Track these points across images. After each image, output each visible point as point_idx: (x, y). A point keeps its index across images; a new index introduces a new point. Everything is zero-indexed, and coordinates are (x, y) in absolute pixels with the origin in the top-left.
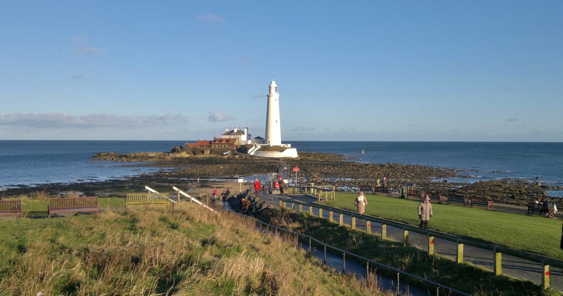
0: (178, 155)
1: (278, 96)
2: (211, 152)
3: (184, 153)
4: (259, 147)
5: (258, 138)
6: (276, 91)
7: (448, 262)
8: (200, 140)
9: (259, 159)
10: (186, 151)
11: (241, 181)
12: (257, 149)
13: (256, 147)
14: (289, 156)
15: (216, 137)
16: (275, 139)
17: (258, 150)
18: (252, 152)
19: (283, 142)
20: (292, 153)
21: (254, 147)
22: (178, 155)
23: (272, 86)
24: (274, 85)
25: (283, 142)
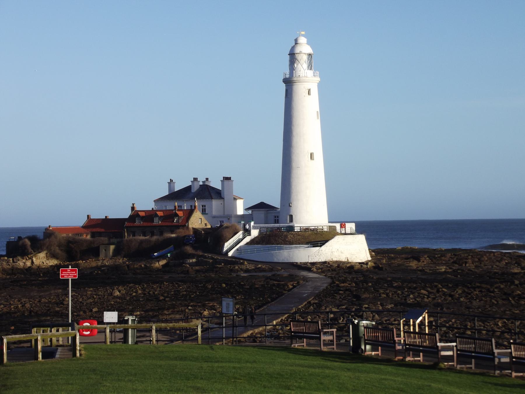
0: (22, 263)
1: (318, 79)
2: (117, 252)
3: (42, 255)
4: (255, 233)
5: (262, 206)
6: (310, 67)
7: (317, 350)
8: (110, 217)
9: (251, 267)
10: (49, 249)
11: (218, 344)
12: (248, 239)
13: (247, 232)
14: (343, 259)
15: (138, 208)
16: (311, 210)
17: (253, 242)
18: (232, 245)
19: (329, 222)
20: (351, 249)
21: (240, 235)
22: (22, 263)
23: (298, 50)
24: (304, 48)
25: (329, 222)
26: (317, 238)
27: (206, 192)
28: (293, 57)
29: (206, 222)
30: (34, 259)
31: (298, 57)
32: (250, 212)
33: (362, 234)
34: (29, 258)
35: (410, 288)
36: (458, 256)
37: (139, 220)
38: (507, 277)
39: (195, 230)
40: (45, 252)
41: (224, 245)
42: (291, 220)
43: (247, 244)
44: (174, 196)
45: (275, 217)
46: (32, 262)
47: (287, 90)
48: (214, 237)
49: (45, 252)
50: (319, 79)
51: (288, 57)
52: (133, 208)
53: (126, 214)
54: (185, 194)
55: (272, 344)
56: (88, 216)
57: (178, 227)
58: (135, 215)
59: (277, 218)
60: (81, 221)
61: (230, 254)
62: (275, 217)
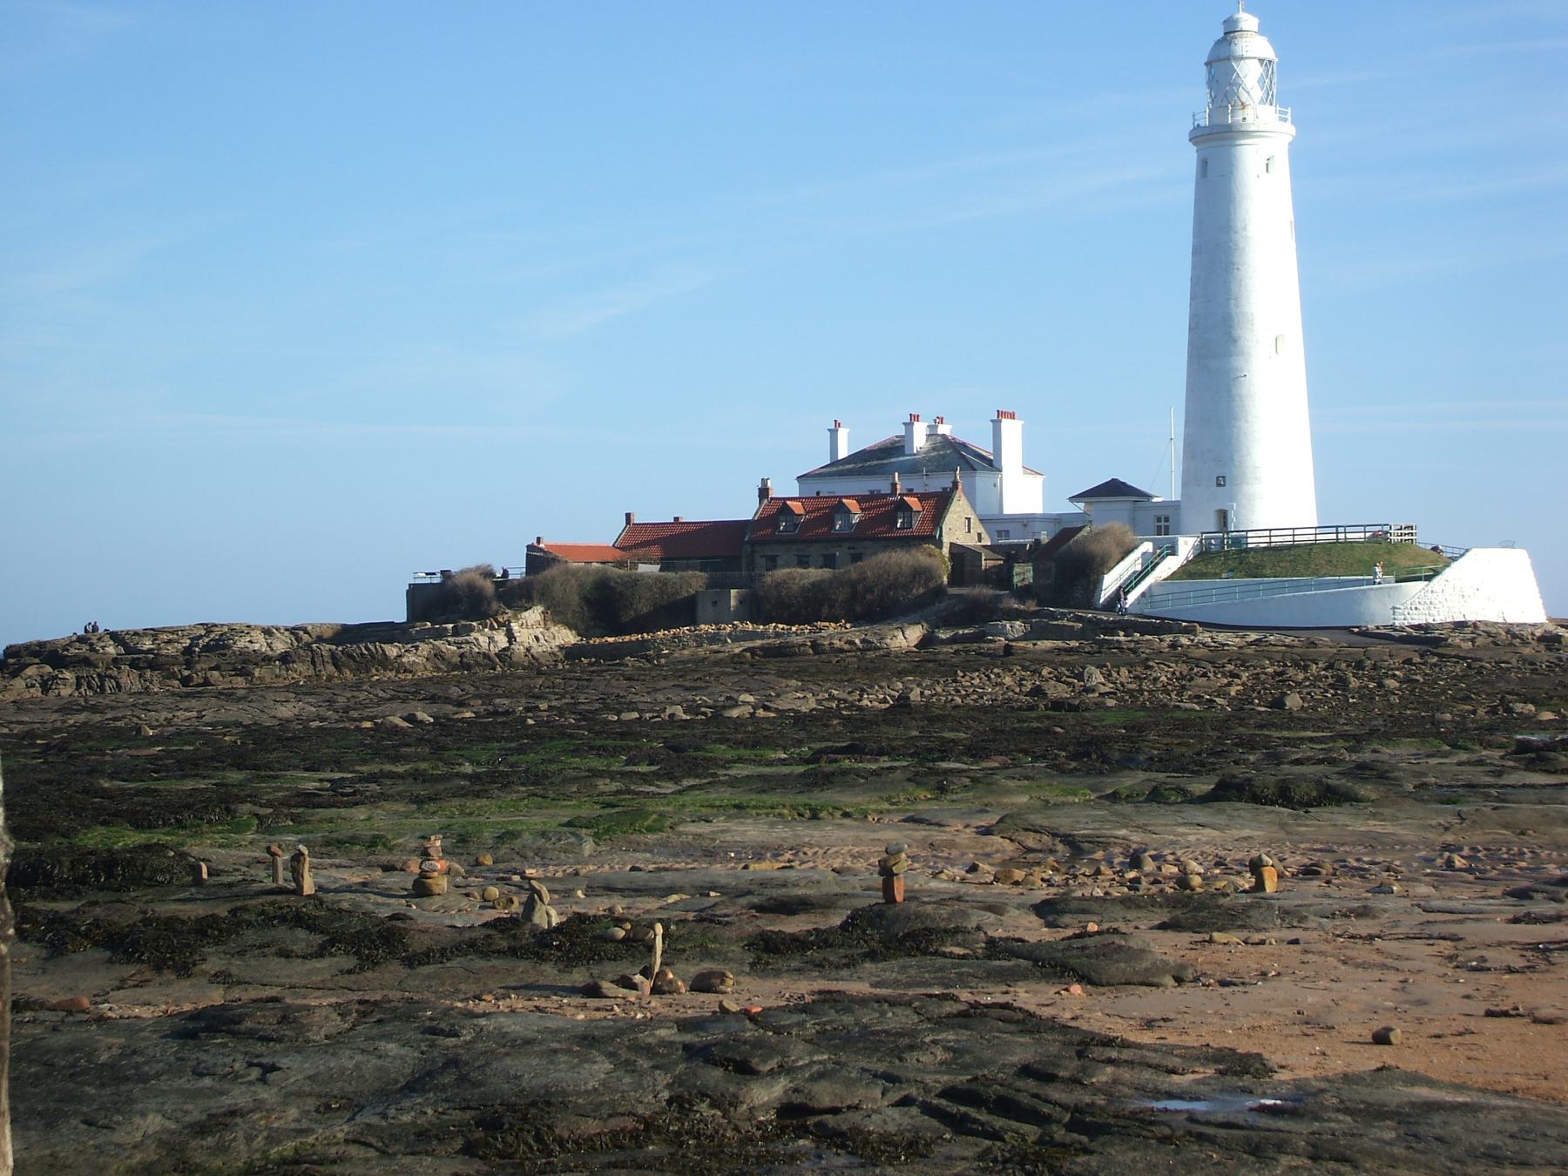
12: (1170, 565)
28: (1220, 63)
29: (981, 529)
30: (515, 626)
32: (1080, 507)
33: (1509, 544)
34: (501, 625)
37: (775, 530)
39: (960, 555)
40: (540, 609)
41: (1098, 583)
43: (1173, 576)
45: (1159, 520)
46: (511, 636)
47: (1204, 166)
49: (540, 609)
50: (1292, 130)
52: (764, 492)
53: (745, 509)
55: (340, 896)
56: (628, 516)
58: (775, 511)
59: (1163, 524)
60: (605, 533)
62: (1159, 520)
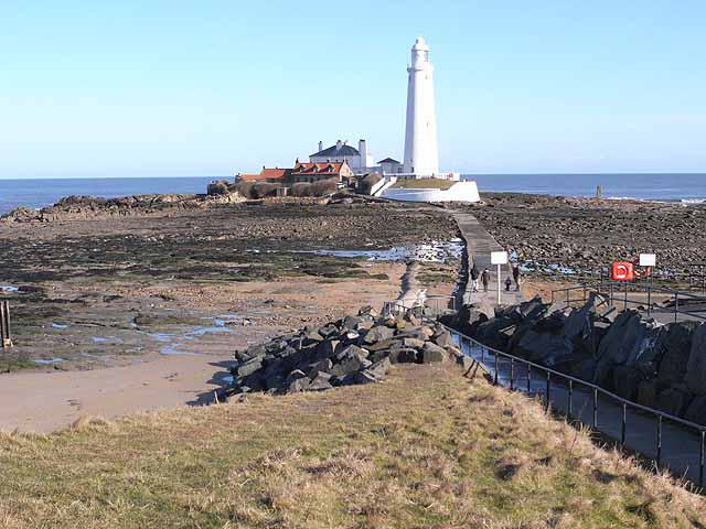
0: (222, 200)
5: (389, 160)
18: (377, 190)
22: (222, 200)
26: (431, 182)
27: (347, 151)
28: (414, 51)
31: (419, 52)
35: (546, 216)
36: (657, 197)
38: (159, 204)
42: (413, 171)
43: (392, 187)
44: (322, 153)
48: (362, 185)
51: (410, 54)
54: (331, 151)
57: (331, 175)
60: (258, 172)
61: (376, 195)
